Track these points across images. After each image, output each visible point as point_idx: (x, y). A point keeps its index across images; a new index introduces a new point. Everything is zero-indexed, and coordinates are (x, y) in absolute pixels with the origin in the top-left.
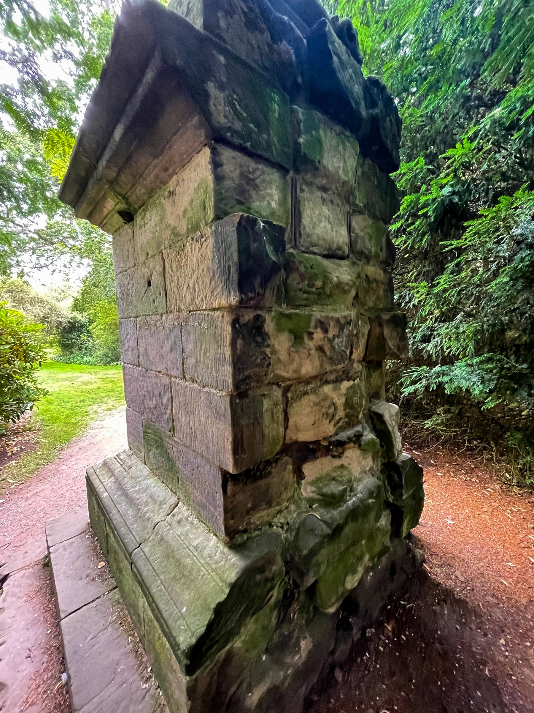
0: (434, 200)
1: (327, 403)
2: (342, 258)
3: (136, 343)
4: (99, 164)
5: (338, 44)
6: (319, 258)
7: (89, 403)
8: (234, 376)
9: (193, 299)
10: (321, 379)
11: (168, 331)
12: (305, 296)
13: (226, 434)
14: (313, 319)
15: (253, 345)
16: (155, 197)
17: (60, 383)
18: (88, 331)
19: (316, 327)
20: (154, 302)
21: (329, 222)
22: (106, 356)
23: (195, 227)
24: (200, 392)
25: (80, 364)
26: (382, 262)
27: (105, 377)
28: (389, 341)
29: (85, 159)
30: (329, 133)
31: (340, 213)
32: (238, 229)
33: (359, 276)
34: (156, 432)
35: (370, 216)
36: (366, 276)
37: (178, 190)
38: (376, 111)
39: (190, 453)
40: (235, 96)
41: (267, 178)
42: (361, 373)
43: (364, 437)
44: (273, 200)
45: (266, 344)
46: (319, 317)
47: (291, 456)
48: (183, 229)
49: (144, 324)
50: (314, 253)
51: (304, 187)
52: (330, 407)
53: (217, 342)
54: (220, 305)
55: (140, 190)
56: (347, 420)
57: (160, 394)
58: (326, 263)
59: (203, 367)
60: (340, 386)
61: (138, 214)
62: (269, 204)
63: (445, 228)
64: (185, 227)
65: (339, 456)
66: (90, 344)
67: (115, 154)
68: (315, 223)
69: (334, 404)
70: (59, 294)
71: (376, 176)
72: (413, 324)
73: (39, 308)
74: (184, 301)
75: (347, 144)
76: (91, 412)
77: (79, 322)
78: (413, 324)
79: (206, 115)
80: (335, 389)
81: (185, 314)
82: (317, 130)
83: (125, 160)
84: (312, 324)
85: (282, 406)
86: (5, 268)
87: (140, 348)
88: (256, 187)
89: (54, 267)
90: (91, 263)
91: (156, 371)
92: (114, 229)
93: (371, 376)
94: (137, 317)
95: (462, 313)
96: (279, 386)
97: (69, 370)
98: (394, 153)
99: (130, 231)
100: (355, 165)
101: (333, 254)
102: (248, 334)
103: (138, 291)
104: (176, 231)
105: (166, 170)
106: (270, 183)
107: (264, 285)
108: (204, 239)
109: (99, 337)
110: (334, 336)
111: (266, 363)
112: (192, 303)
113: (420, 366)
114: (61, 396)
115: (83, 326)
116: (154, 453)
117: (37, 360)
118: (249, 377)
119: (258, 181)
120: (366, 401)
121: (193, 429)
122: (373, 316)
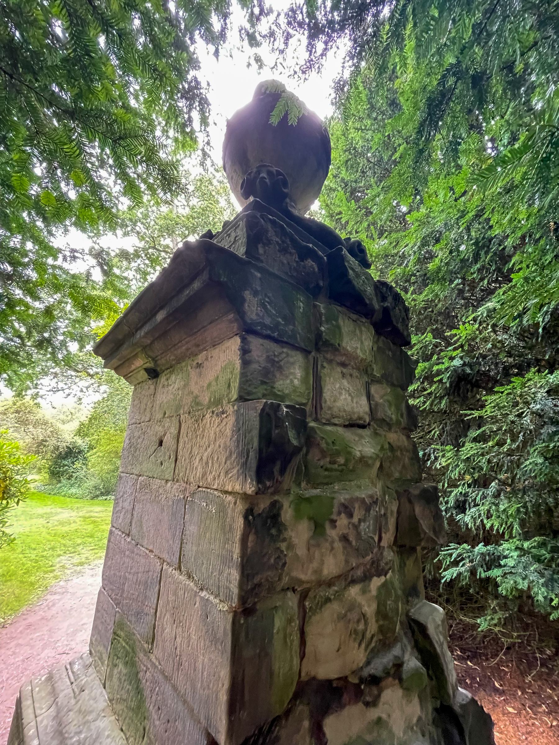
0: (447, 369)
1: (354, 616)
2: (363, 427)
3: (132, 506)
4: (139, 332)
5: (351, 261)
6: (340, 430)
7: (59, 552)
8: (241, 586)
9: (204, 475)
10: (348, 579)
11: (170, 503)
12: (326, 473)
13: (222, 674)
14: (336, 502)
15: (267, 540)
16: (183, 364)
17: (34, 521)
18: (85, 458)
19: (339, 513)
20: (162, 464)
21: (350, 395)
22: (96, 488)
23: (218, 402)
24: (195, 596)
25: (65, 496)
26: (405, 429)
27: (87, 515)
28: (421, 522)
29: (126, 328)
30: (347, 321)
31: (359, 384)
32: (261, 415)
33: (382, 448)
34: (129, 636)
35: (387, 385)
36: (389, 443)
37: (206, 364)
38: (386, 304)
39: (168, 689)
40: (267, 300)
41: (291, 360)
42: (393, 564)
43: (405, 667)
44: (296, 378)
45: (281, 537)
46: (343, 501)
47: (308, 704)
48: (205, 399)
49: (145, 486)
50: (335, 425)
51: (325, 364)
52: (358, 621)
53: (225, 534)
54: (233, 489)
55: (170, 357)
56: (381, 637)
57: (146, 582)
58: (349, 435)
59: (205, 562)
60: (369, 585)
61: (163, 374)
62: (292, 381)
63: (461, 391)
64: (207, 399)
65: (373, 704)
66: (81, 474)
67: (155, 329)
68: (336, 396)
69: (364, 615)
70: (67, 416)
71: (390, 349)
72: (443, 486)
73: (40, 430)
74: (194, 473)
75: (363, 329)
76: (58, 566)
77: (78, 448)
78: (443, 486)
79: (241, 314)
80: (364, 591)
81: (193, 488)
82: (337, 320)
83: (162, 333)
84: (335, 510)
85: (298, 622)
86: (22, 390)
87: (135, 513)
88: (280, 368)
89: (71, 391)
90: (108, 390)
91: (147, 549)
92: (138, 382)
93: (405, 564)
94: (140, 475)
95: (497, 481)
96: (294, 590)
97: (50, 503)
98: (405, 333)
99: (152, 387)
100: (371, 344)
101: (354, 425)
102: (262, 523)
103: (147, 449)
104: (197, 400)
105: (198, 346)
106: (293, 364)
107: (282, 471)
108: (225, 415)
109: (96, 466)
110: (360, 521)
111: (281, 564)
112: (203, 477)
113: (460, 544)
114: (29, 540)
115: (80, 452)
116: (120, 673)
117: (17, 497)
118: (259, 585)
119: (282, 363)
120: (402, 603)
121: (178, 649)
122: (401, 490)
